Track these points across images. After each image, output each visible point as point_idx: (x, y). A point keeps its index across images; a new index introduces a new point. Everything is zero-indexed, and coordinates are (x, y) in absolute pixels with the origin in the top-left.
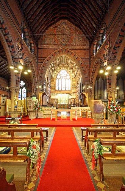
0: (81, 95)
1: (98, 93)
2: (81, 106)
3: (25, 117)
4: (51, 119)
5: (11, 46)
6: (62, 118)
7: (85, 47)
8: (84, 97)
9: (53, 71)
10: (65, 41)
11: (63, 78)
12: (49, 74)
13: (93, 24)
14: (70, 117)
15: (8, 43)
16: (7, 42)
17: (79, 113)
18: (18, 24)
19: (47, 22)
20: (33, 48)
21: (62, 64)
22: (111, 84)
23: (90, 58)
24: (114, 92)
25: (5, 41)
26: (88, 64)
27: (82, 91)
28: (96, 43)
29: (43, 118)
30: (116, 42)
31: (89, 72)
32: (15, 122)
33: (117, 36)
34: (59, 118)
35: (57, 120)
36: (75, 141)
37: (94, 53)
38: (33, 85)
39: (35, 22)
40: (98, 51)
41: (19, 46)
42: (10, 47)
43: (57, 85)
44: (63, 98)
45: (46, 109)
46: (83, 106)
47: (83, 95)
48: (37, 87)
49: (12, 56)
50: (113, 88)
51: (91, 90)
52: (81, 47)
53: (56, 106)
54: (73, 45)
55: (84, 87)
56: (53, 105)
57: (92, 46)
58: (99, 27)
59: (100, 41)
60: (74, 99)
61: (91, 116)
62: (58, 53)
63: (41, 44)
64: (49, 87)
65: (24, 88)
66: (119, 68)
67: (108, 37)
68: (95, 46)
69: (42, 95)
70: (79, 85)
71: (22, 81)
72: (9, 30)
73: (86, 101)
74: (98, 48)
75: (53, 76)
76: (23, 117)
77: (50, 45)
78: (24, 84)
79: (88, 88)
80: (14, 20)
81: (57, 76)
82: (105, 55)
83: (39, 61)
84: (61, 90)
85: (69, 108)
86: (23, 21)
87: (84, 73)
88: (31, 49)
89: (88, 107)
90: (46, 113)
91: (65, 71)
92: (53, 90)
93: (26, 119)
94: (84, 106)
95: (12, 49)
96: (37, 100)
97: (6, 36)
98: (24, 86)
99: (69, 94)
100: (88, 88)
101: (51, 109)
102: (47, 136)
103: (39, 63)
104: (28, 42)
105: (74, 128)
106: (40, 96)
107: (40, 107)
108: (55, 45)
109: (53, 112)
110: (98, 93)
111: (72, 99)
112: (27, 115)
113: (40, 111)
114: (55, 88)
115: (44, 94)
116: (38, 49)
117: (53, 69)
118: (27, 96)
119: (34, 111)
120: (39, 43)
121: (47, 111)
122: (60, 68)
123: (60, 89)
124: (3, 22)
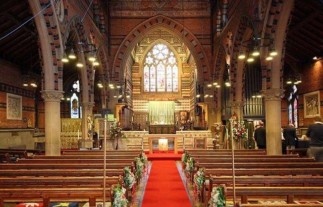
6: (160, 150)
11: (161, 62)
22: (269, 81)
24: (239, 107)
26: (210, 46)
31: (212, 62)
43: (145, 80)
44: (160, 110)
45: (129, 136)
48: (100, 86)
49: (48, 24)
52: (195, 14)
54: (178, 9)
60: (186, 113)
62: (149, 26)
75: (137, 60)
77: (133, 10)
81: (147, 59)
84: (156, 92)
85: (174, 133)
99: (176, 100)
103: (112, 47)
106: (118, 111)
107: (122, 132)
111: (181, 113)
114: (141, 87)
119: (111, 139)
121: (133, 140)
123: (153, 90)
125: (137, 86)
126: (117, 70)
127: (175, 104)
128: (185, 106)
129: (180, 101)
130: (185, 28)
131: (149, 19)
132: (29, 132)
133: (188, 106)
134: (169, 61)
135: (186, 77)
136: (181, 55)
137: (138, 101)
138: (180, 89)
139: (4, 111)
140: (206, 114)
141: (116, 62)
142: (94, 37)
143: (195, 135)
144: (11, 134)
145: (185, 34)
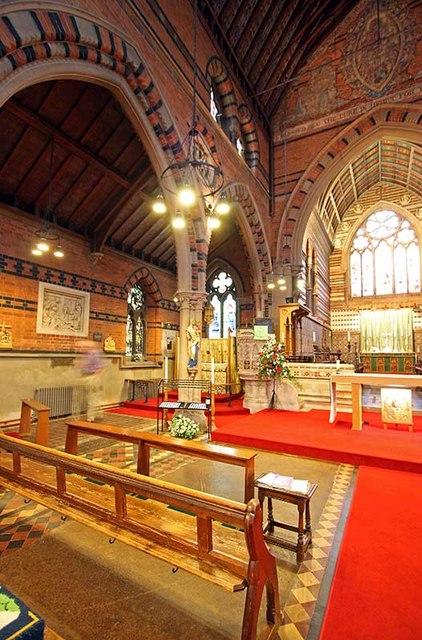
3: (229, 401)
4: (332, 420)
5: (173, 148)
6: (386, 418)
9: (335, 225)
12: (321, 237)
15: (160, 139)
16: (158, 134)
18: (193, 66)
19: (304, 29)
20: (253, 149)
21: (372, 188)
25: (152, 134)
29: (296, 408)
32: (189, 420)
34: (372, 418)
35: (358, 424)
38: (259, 282)
39: (256, 51)
41: (201, 146)
42: (169, 151)
48: (271, 286)
53: (357, 366)
56: (339, 355)
63: (282, 128)
64: (320, 289)
65: (230, 296)
69: (293, 318)
71: (222, 275)
72: (161, 92)
75: (337, 244)
76: (217, 401)
78: (229, 282)
80: (179, 57)
81: (355, 241)
83: (276, 184)
84: (375, 296)
86: (216, 58)
88: (247, 153)
90: (307, 389)
91: (393, 214)
92: (336, 297)
93: (235, 408)
95: (168, 139)
96: (273, 336)
97: (152, 115)
98: (230, 290)
101: (328, 375)
102: (304, 530)
104: (233, 126)
106: (283, 321)
107: (284, 365)
108: (338, 110)
109: (337, 389)
112: (238, 391)
113: (284, 380)
114: (346, 290)
115: (300, 313)
116: (272, 147)
117: (335, 217)
118: (240, 325)
120: (276, 128)
121: (315, 384)
122: (365, 204)
123: (369, 293)
124: (142, 66)
125: (338, 289)
126: (288, 241)
131: (355, 123)
132: (111, 360)
134: (400, 239)
137: (341, 313)
139: (31, 316)
141: (286, 226)
142: (213, 149)
144: (49, 362)
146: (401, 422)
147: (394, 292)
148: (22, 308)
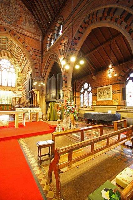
0: (30, 92)
1: (50, 92)
2: (30, 107)
7: (37, 37)
8: (35, 95)
10: (10, 18)
13: (48, 13)
14: (14, 123)
17: (28, 115)
22: (67, 83)
23: (42, 51)
27: (32, 89)
28: (50, 36)
30: (74, 38)
33: (76, 32)
36: (27, 167)
37: (48, 47)
40: (51, 46)
46: (32, 107)
47: (33, 93)
50: (69, 87)
51: (42, 87)
52: (32, 36)
54: (22, 29)
55: (35, 83)
57: (46, 38)
58: (54, 20)
59: (55, 35)
60: (19, 98)
61: (43, 119)
66: (82, 62)
67: (65, 31)
68: (49, 40)
70: (28, 81)
73: (37, 100)
74: (52, 42)
79: (39, 85)
82: (61, 50)
85: (12, 110)
87: (34, 66)
89: (39, 108)
94: (34, 107)
99: (13, 91)
100: (39, 85)
105: (21, 141)
110: (50, 92)
111: (16, 98)
127: (14, 93)
128: (18, 95)
129: (16, 92)
130: (25, 42)
133: (20, 95)
135: (20, 80)
136: (18, 68)
138: (16, 86)
140: (38, 97)
143: (31, 111)
145: (26, 45)
146: (5, 125)
147: (1, 85)
148: (114, 91)
